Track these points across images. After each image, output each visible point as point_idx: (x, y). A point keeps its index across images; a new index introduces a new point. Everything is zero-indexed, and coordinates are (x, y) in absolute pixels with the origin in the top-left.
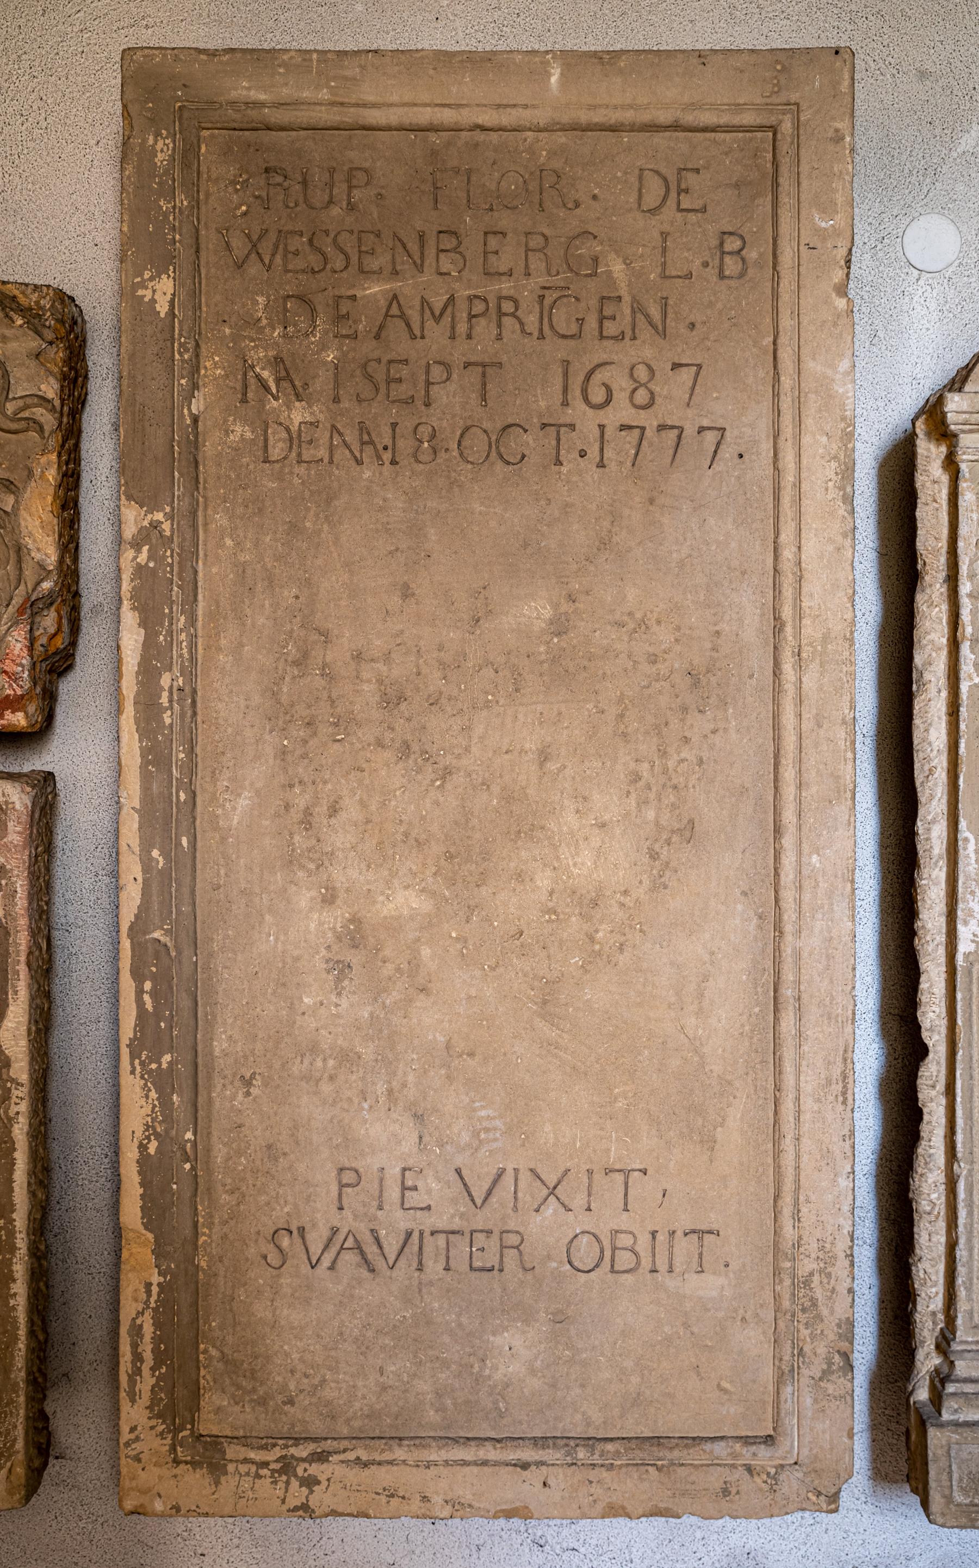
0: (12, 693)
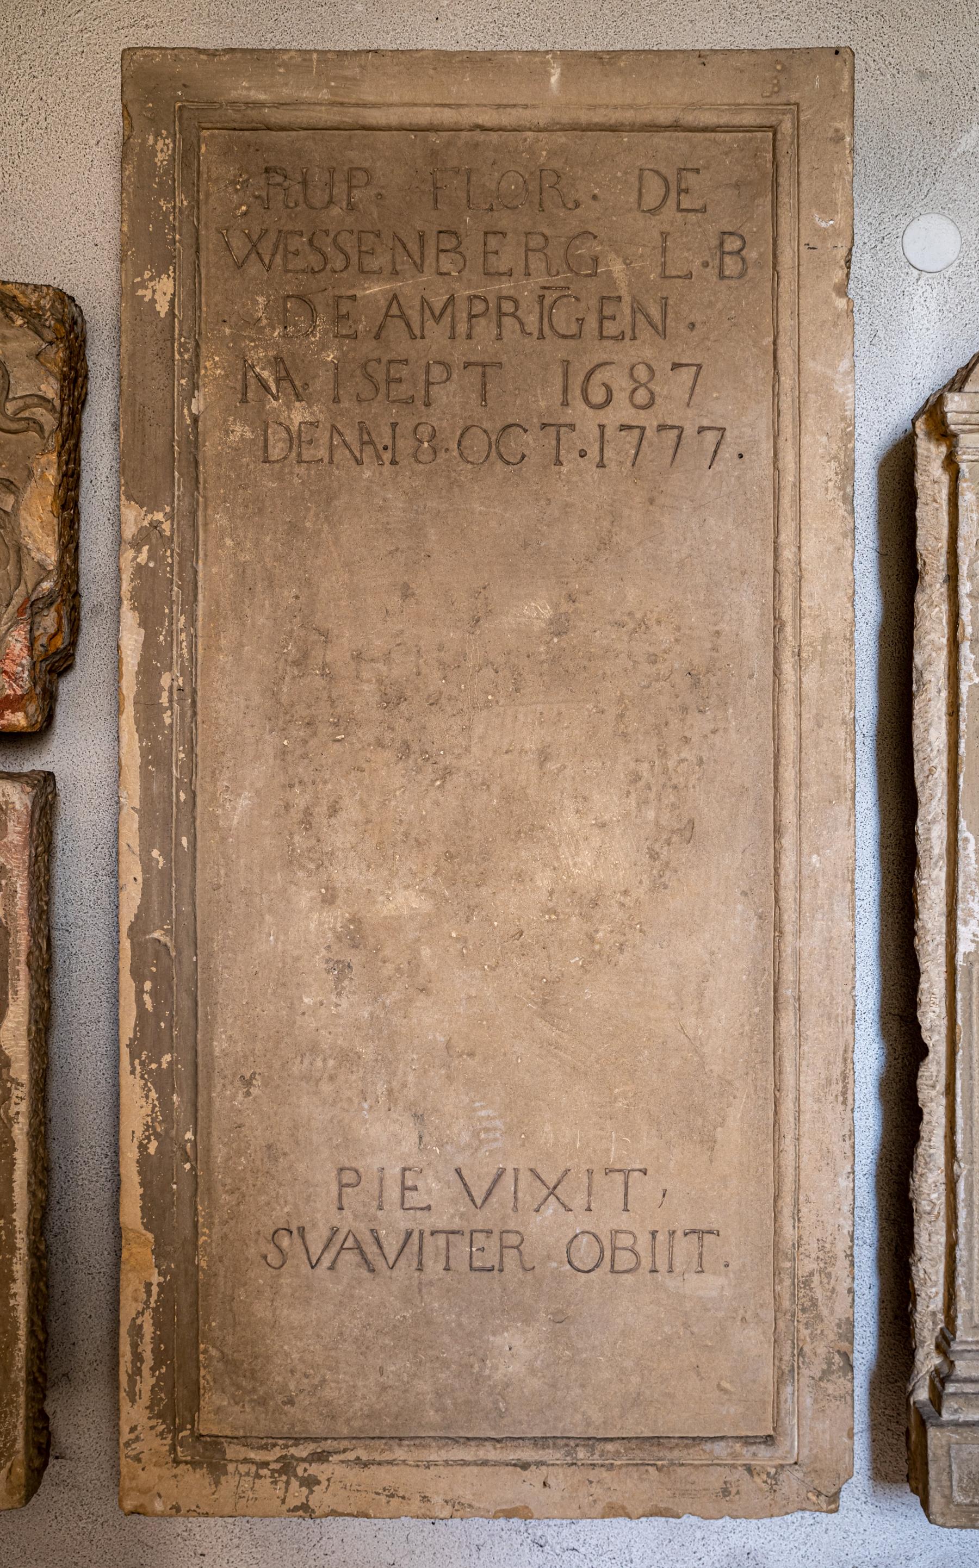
0: (12, 693)
